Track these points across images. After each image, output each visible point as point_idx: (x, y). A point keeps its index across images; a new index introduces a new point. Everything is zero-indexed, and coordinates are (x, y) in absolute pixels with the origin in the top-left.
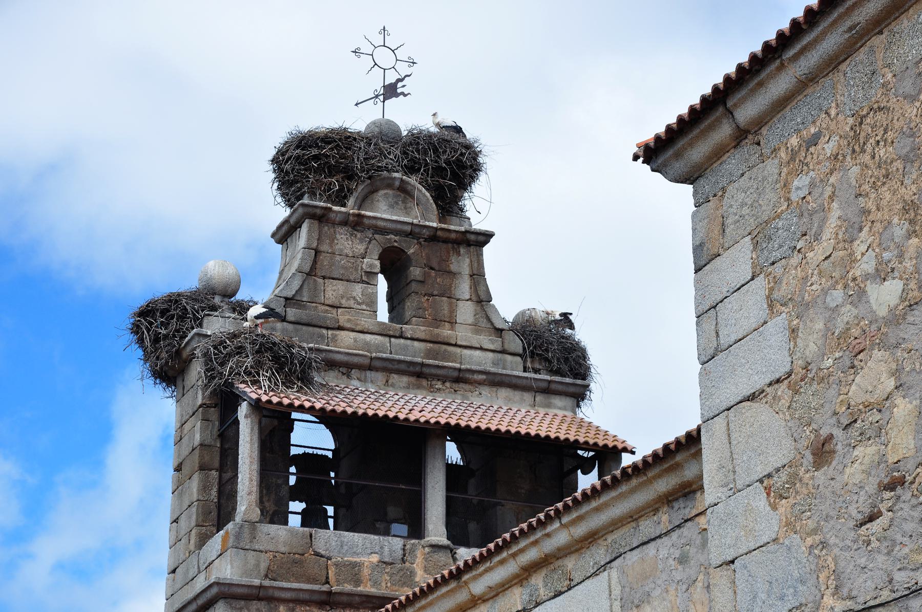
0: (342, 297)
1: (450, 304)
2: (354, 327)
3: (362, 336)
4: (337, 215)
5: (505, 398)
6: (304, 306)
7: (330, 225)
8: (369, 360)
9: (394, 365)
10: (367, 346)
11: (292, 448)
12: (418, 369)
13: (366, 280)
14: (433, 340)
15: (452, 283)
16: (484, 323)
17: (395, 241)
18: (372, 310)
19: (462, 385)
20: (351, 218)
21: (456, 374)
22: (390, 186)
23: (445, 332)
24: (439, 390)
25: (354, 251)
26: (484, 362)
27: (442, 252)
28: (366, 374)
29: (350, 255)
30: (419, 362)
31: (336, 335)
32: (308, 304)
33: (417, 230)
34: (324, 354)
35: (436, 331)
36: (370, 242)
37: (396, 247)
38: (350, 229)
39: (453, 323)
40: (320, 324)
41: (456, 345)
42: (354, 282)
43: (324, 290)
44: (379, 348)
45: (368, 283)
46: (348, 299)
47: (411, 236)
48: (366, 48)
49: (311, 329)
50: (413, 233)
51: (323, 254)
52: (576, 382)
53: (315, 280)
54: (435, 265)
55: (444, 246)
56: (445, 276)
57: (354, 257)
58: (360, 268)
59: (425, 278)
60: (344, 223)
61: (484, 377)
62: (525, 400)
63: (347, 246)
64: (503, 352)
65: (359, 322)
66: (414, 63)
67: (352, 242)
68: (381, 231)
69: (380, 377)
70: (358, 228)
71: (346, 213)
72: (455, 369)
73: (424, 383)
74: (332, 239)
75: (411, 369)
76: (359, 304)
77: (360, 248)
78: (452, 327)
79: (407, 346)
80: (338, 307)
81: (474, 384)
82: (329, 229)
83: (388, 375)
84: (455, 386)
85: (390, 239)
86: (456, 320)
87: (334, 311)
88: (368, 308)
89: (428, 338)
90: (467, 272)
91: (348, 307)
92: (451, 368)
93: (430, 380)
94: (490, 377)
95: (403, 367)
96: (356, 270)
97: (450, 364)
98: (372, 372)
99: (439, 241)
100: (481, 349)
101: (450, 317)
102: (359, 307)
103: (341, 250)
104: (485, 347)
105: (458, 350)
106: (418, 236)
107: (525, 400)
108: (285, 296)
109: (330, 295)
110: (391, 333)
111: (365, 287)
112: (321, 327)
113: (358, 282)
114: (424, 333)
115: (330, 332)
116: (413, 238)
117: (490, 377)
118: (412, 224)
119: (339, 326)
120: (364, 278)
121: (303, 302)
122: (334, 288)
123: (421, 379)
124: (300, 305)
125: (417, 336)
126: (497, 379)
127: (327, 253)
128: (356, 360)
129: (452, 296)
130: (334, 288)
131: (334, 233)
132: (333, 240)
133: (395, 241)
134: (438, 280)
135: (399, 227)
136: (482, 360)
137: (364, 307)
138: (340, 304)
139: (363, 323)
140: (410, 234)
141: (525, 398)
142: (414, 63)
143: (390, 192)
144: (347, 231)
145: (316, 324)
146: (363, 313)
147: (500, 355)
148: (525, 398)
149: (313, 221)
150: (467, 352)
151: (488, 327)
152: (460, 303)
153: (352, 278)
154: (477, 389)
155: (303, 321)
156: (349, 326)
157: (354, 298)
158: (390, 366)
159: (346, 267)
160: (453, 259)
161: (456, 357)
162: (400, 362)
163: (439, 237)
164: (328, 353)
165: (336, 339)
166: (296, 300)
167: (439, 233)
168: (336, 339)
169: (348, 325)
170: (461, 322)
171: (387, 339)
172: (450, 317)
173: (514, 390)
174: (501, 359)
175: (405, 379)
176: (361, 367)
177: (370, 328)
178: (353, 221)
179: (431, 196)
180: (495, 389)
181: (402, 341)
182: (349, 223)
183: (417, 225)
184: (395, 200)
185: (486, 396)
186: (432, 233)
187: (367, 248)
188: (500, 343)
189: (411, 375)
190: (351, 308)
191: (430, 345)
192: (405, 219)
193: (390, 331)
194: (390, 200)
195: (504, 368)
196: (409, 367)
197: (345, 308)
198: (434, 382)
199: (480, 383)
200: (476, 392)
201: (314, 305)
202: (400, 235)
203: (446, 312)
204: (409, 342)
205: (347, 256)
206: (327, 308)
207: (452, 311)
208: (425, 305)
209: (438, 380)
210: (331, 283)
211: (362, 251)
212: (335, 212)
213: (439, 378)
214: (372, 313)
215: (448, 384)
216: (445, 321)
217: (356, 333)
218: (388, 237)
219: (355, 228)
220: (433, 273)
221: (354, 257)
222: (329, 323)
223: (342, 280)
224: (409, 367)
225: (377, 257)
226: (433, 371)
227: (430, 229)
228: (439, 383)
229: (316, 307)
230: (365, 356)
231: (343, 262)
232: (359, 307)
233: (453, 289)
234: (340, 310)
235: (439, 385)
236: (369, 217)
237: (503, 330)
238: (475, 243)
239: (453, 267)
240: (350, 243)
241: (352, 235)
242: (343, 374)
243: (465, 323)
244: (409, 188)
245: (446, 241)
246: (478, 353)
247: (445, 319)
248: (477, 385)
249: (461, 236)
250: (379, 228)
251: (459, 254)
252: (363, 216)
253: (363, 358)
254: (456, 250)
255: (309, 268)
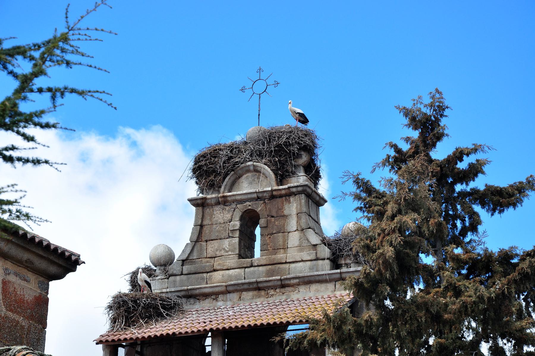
0: (217, 250)
1: (284, 237)
2: (222, 268)
3: (227, 272)
4: (211, 200)
5: (315, 291)
6: (194, 262)
7: (210, 207)
8: (225, 288)
9: (240, 287)
10: (230, 278)
11: (206, 347)
12: (255, 286)
13: (231, 235)
14: (272, 263)
15: (285, 223)
16: (305, 244)
17: (249, 206)
18: (235, 254)
19: (287, 289)
20: (220, 200)
21: (279, 283)
22: (248, 171)
23: (280, 256)
24: (272, 295)
25: (224, 219)
26: (303, 270)
27: (279, 204)
28: (227, 296)
29: (222, 223)
30: (254, 281)
31: (211, 276)
32: (197, 260)
33: (260, 195)
34: (198, 291)
35: (273, 256)
36: (234, 211)
37: (250, 209)
38: (222, 206)
39: (285, 248)
40: (202, 271)
41: (286, 263)
42: (224, 239)
43: (207, 249)
44: (237, 277)
45: (233, 237)
46: (221, 251)
47: (259, 200)
48: (264, 76)
49: (197, 275)
50: (259, 197)
51: (206, 227)
52: (357, 270)
53: (201, 244)
54: (274, 214)
55: (280, 200)
56: (280, 219)
57: (224, 223)
58: (227, 229)
59: (267, 224)
60: (218, 203)
61: (297, 280)
62: (328, 289)
63: (220, 217)
64: (317, 259)
65: (225, 264)
66: (278, 83)
67: (223, 214)
68: (241, 202)
69: (235, 296)
70: (227, 204)
71: (215, 197)
72: (278, 280)
73: (263, 293)
74: (211, 215)
75: (251, 286)
76: (227, 252)
77: (228, 216)
78: (285, 251)
79: (254, 271)
80: (215, 257)
81: (294, 286)
82: (209, 210)
83: (241, 293)
84: (283, 290)
85: (246, 205)
86: (288, 246)
87: (212, 260)
88: (233, 253)
89: (268, 263)
90: (295, 213)
91: (221, 255)
92: (275, 280)
93: (266, 290)
94: (301, 280)
95: (246, 287)
96: (225, 231)
97: (274, 278)
98: (231, 294)
99: (277, 198)
100: (302, 261)
101: (284, 245)
102: (227, 254)
103: (217, 221)
104: (304, 259)
105: (287, 266)
106: (264, 198)
107: (328, 289)
108: (182, 259)
109: (210, 251)
110: (245, 265)
111: (231, 240)
112: (203, 273)
113: (227, 238)
114: (265, 261)
115: (209, 274)
116: (260, 201)
117: (301, 280)
118: (256, 192)
119: (214, 269)
120: (230, 235)
121: (194, 259)
122: (213, 246)
123: (260, 291)
124: (192, 262)
125: (261, 263)
126: (306, 280)
127: (209, 225)
128: (217, 290)
129: (285, 231)
130: (213, 246)
131: (213, 211)
132: (212, 216)
133: (249, 206)
134: (276, 223)
135: (249, 196)
136: (303, 268)
137: (230, 253)
138: (216, 255)
139: (228, 263)
140: (258, 198)
141: (328, 287)
142: (278, 83)
143: (249, 174)
144: (220, 208)
145: (200, 272)
146: (229, 257)
147: (314, 262)
148: (328, 287)
149: (199, 208)
150: (293, 265)
151: (308, 245)
152: (290, 234)
153: (223, 237)
154: (297, 289)
155: (192, 272)
156: (219, 268)
157: (224, 249)
158: (238, 288)
159: (220, 231)
160: (286, 206)
161: (285, 270)
162: (243, 284)
163: (275, 195)
164: (200, 290)
165: (211, 278)
166: (190, 260)
167: (274, 193)
168: (211, 278)
169: (218, 268)
170: (290, 246)
171: (243, 270)
172: (284, 245)
173: (321, 283)
174: (315, 265)
175: (251, 294)
176: (222, 293)
177: (232, 266)
178: (222, 201)
179: (272, 170)
180: (308, 286)
181: (252, 269)
182: (221, 202)
183: (259, 192)
184: (253, 178)
185: (303, 292)
186: (270, 194)
187: (232, 215)
188: (314, 254)
189: (254, 290)
190: (222, 256)
191: (270, 267)
192: (251, 190)
193: (244, 264)
194: (250, 179)
195: (317, 271)
196: (249, 286)
197: (219, 257)
198: (269, 291)
199: (298, 284)
200: (296, 291)
201: (201, 259)
202: (253, 201)
203: (281, 243)
204: (256, 268)
205: (220, 223)
206: (208, 259)
207: (285, 241)
208: (268, 241)
209: (272, 289)
210: (211, 243)
211: (230, 218)
212: (209, 199)
213: (269, 288)
214: (234, 255)
215: (278, 290)
216: (280, 249)
217: (224, 271)
218: (245, 204)
219: (226, 204)
220: (273, 219)
221: (224, 223)
222: (207, 269)
223: (217, 239)
224: (249, 286)
225: (238, 219)
226: (265, 285)
227: (268, 192)
228: (272, 290)
229: (201, 261)
230: (222, 286)
231: (217, 228)
232: (227, 254)
233: (285, 226)
234: (216, 259)
235: (272, 292)
236: (230, 196)
237: (316, 245)
238: (298, 193)
239: (286, 212)
240: (222, 215)
241: (223, 209)
242: (214, 299)
243: (293, 246)
244: (259, 169)
245: (281, 196)
246: (301, 264)
247: (280, 247)
248: (296, 286)
249: (288, 191)
250: (239, 200)
251: (289, 202)
252: (226, 197)
253: (221, 287)
254: (288, 200)
255: (196, 238)
